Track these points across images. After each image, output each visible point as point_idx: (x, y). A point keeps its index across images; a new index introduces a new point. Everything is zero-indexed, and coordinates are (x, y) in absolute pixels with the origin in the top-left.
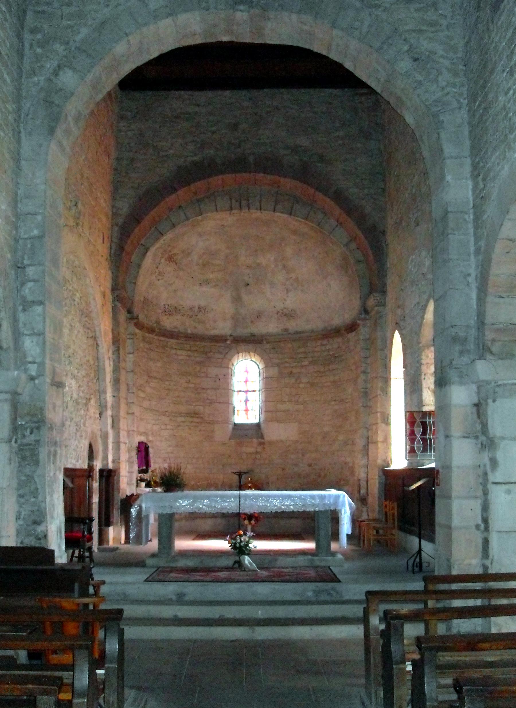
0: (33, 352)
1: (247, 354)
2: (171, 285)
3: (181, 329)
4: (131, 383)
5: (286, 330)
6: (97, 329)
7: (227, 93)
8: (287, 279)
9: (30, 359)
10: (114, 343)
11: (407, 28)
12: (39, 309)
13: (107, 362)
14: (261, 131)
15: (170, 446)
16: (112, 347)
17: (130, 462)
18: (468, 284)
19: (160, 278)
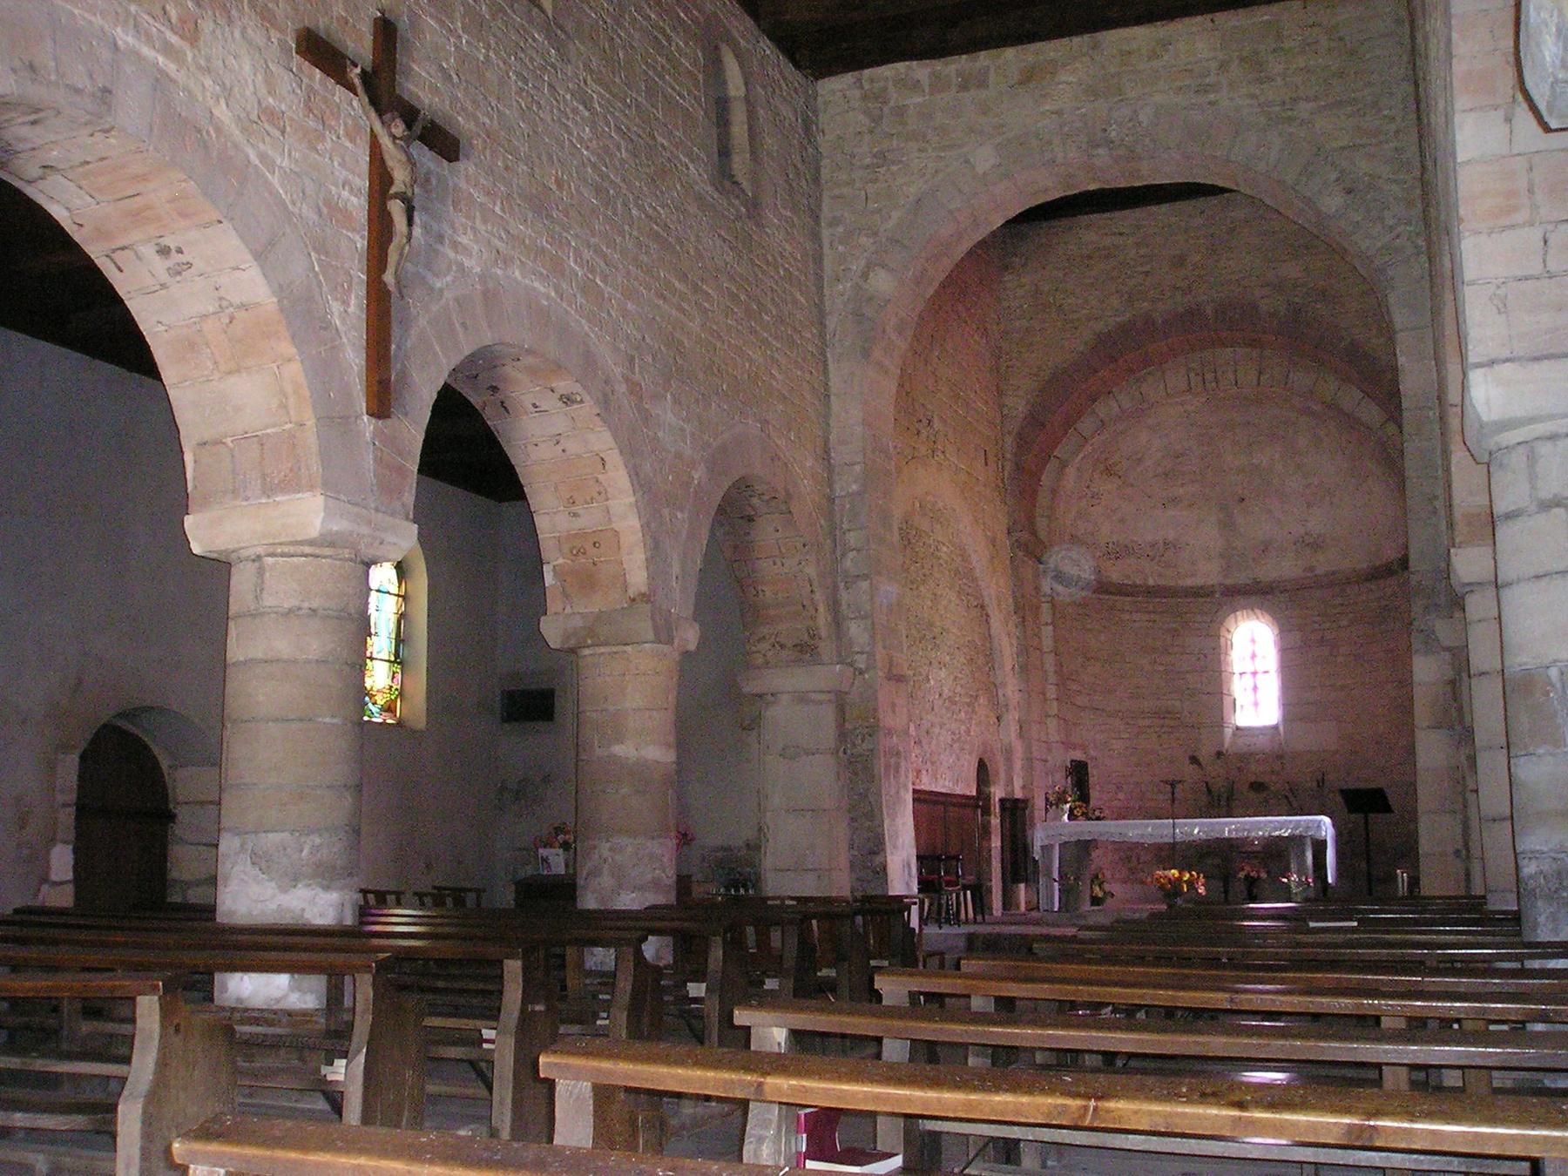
0: (861, 640)
1: (1250, 612)
9: (857, 649)
11: (1335, 145)
12: (865, 585)
18: (1435, 512)
19: (1095, 501)
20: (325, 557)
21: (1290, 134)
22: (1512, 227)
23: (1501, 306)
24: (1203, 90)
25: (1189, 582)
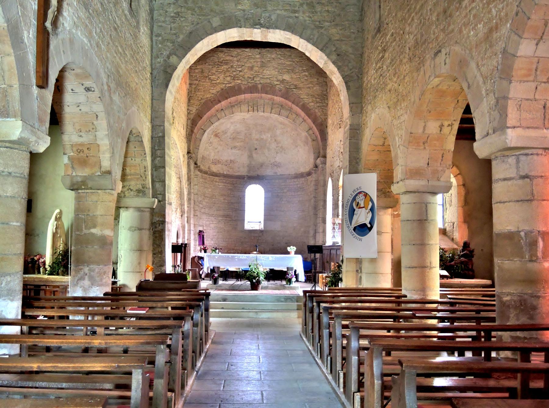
2: (216, 149)
3: (222, 172)
4: (196, 200)
5: (276, 173)
6: (181, 174)
7: (247, 50)
8: (277, 147)
9: (159, 193)
10: (188, 180)
13: (185, 189)
14: (265, 72)
15: (215, 232)
16: (187, 182)
17: (195, 240)
20: (15, 149)
21: (321, 33)
22: (528, 81)
23: (519, 108)
24: (295, 12)
25: (237, 174)
